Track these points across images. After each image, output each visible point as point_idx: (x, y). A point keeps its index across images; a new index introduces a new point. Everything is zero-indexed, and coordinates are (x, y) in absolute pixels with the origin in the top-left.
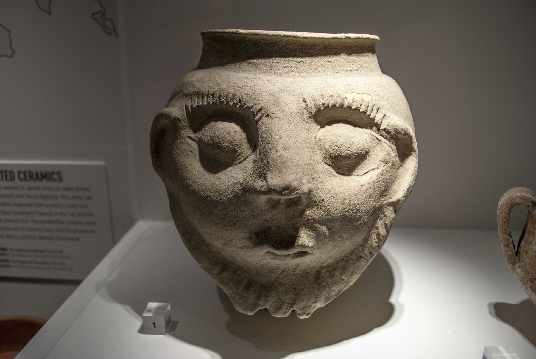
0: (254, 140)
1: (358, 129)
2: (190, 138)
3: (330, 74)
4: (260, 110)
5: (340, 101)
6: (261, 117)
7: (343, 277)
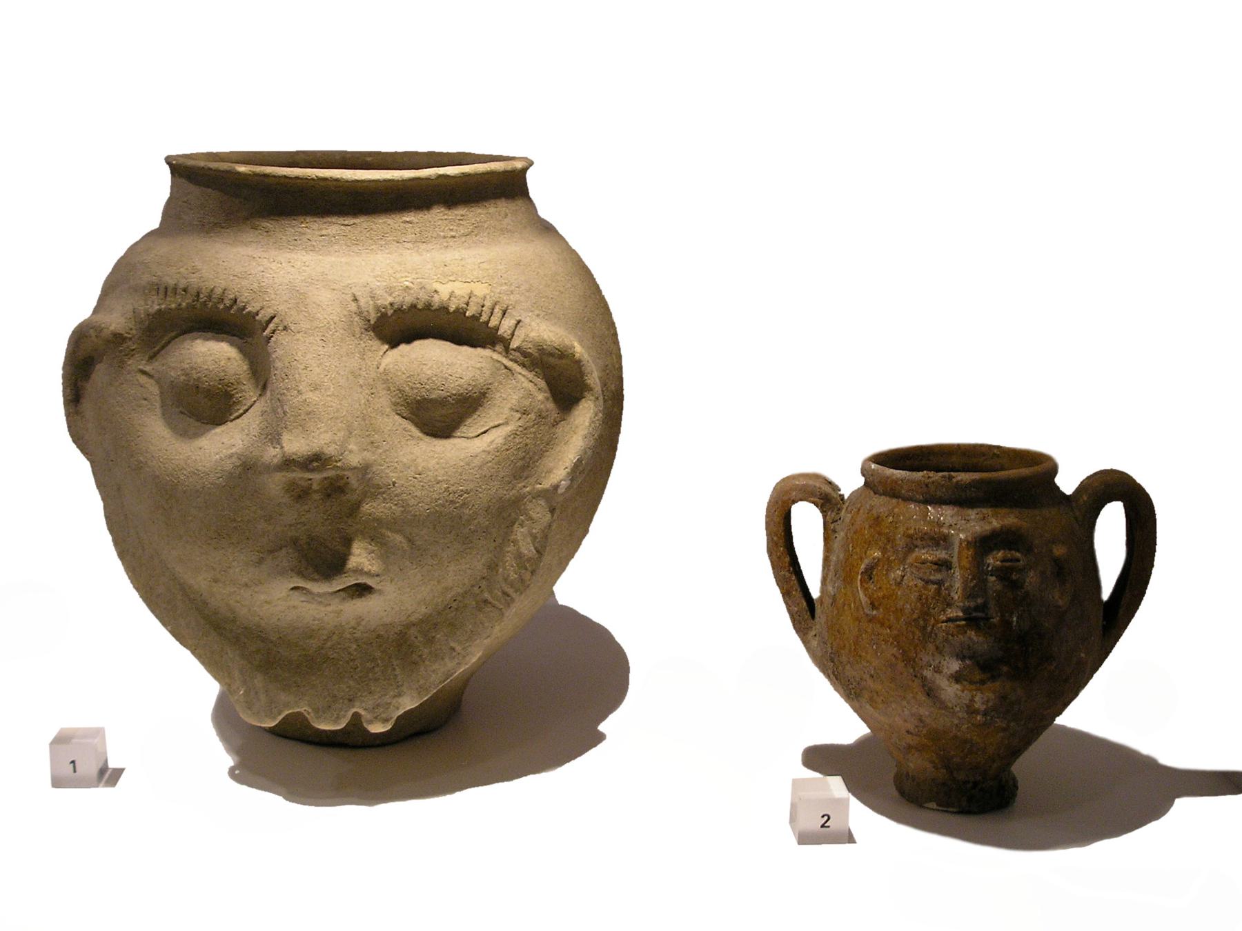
0: (261, 370)
1: (466, 350)
2: (144, 372)
3: (409, 245)
4: (273, 318)
5: (424, 297)
6: (274, 332)
7: (453, 644)
